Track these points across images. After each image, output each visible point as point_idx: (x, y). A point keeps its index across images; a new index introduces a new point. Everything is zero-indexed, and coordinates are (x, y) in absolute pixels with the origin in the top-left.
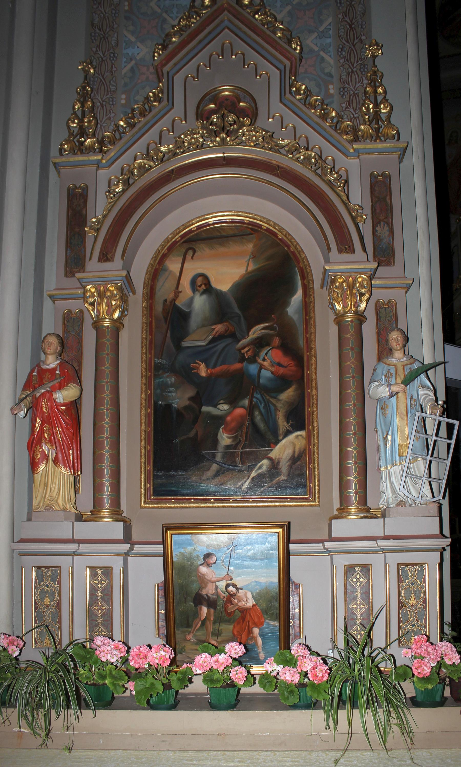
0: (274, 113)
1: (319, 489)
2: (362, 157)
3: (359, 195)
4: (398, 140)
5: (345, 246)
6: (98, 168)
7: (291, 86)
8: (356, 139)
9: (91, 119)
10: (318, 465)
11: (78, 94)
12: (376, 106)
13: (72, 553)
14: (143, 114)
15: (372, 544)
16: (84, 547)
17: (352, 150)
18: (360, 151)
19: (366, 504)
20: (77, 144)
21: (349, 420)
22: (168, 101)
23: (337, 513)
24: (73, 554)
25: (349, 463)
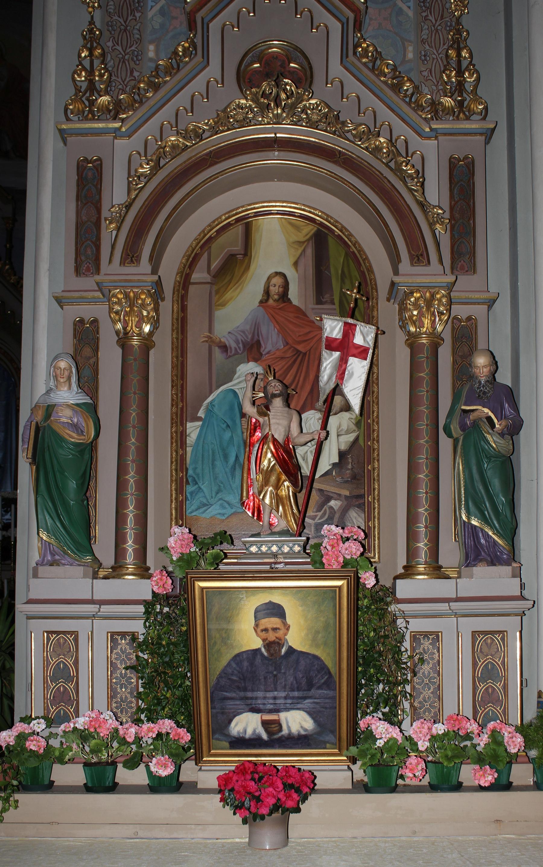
0: (338, 81)
1: (379, 543)
2: (440, 138)
3: (436, 192)
4: (484, 118)
5: (419, 256)
6: (115, 138)
7: (356, 47)
8: (436, 116)
9: (103, 71)
10: (379, 513)
11: (84, 38)
12: (460, 73)
13: (92, 616)
14: (170, 70)
15: (444, 607)
16: (106, 609)
17: (427, 130)
18: (439, 131)
19: (437, 560)
20: (87, 103)
21: (420, 476)
22: (203, 57)
23: (403, 571)
24: (93, 617)
25: (418, 527)
